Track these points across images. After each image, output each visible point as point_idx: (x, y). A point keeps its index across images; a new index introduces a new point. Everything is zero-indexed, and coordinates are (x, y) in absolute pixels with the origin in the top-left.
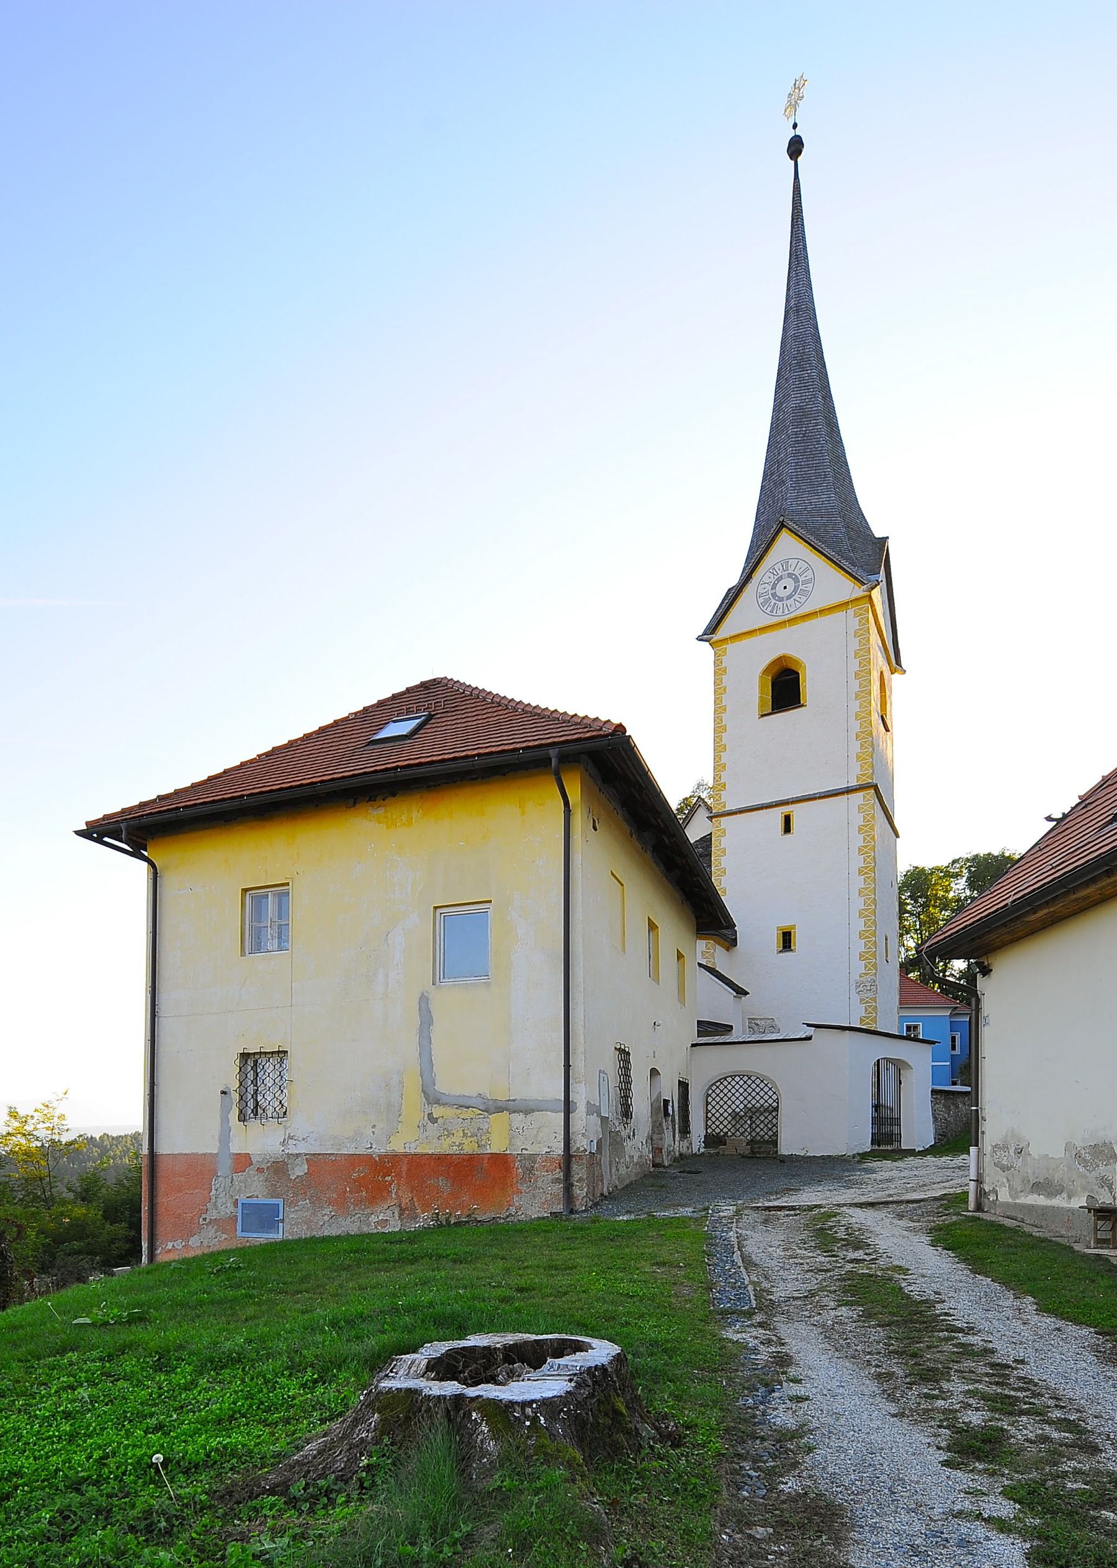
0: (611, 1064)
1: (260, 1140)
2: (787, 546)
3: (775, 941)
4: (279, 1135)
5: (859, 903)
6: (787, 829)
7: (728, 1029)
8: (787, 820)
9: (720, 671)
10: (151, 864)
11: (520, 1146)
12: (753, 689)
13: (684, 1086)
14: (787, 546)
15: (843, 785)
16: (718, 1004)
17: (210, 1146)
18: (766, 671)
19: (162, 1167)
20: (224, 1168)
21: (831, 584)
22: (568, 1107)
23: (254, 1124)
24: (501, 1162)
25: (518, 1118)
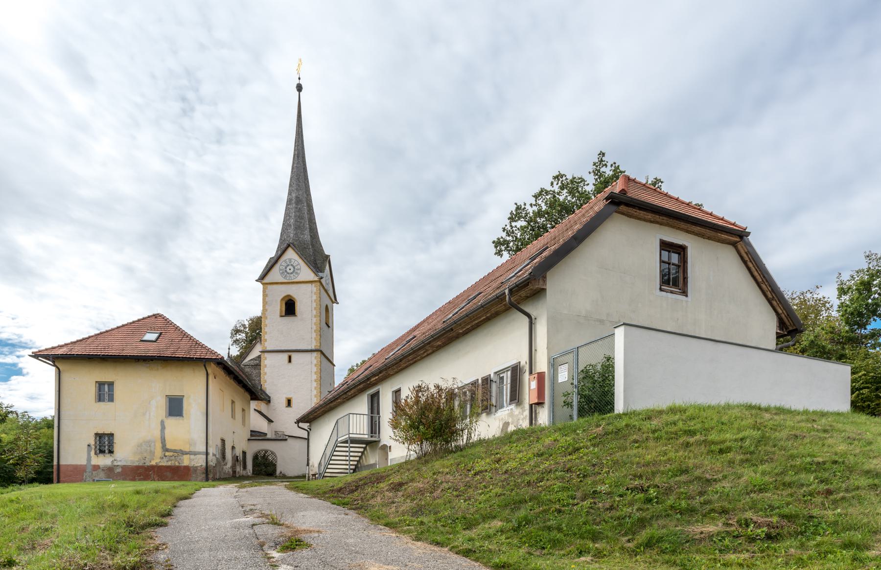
0: (219, 443)
1: (104, 461)
2: (291, 254)
3: (285, 403)
4: (111, 459)
5: (315, 392)
6: (290, 361)
7: (266, 434)
8: (290, 357)
9: (265, 295)
10: (57, 367)
11: (192, 464)
12: (278, 307)
13: (244, 453)
14: (291, 254)
15: (309, 348)
16: (261, 425)
17: (83, 462)
18: (282, 299)
19: (62, 469)
20: (89, 469)
21: (306, 273)
22: (207, 454)
23: (101, 455)
24: (187, 468)
25: (192, 457)
